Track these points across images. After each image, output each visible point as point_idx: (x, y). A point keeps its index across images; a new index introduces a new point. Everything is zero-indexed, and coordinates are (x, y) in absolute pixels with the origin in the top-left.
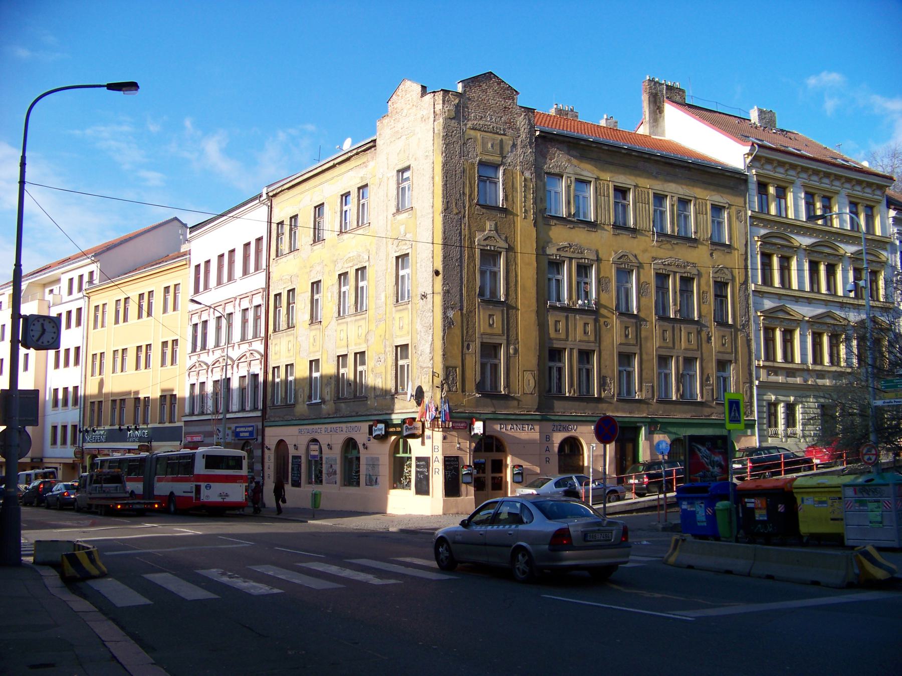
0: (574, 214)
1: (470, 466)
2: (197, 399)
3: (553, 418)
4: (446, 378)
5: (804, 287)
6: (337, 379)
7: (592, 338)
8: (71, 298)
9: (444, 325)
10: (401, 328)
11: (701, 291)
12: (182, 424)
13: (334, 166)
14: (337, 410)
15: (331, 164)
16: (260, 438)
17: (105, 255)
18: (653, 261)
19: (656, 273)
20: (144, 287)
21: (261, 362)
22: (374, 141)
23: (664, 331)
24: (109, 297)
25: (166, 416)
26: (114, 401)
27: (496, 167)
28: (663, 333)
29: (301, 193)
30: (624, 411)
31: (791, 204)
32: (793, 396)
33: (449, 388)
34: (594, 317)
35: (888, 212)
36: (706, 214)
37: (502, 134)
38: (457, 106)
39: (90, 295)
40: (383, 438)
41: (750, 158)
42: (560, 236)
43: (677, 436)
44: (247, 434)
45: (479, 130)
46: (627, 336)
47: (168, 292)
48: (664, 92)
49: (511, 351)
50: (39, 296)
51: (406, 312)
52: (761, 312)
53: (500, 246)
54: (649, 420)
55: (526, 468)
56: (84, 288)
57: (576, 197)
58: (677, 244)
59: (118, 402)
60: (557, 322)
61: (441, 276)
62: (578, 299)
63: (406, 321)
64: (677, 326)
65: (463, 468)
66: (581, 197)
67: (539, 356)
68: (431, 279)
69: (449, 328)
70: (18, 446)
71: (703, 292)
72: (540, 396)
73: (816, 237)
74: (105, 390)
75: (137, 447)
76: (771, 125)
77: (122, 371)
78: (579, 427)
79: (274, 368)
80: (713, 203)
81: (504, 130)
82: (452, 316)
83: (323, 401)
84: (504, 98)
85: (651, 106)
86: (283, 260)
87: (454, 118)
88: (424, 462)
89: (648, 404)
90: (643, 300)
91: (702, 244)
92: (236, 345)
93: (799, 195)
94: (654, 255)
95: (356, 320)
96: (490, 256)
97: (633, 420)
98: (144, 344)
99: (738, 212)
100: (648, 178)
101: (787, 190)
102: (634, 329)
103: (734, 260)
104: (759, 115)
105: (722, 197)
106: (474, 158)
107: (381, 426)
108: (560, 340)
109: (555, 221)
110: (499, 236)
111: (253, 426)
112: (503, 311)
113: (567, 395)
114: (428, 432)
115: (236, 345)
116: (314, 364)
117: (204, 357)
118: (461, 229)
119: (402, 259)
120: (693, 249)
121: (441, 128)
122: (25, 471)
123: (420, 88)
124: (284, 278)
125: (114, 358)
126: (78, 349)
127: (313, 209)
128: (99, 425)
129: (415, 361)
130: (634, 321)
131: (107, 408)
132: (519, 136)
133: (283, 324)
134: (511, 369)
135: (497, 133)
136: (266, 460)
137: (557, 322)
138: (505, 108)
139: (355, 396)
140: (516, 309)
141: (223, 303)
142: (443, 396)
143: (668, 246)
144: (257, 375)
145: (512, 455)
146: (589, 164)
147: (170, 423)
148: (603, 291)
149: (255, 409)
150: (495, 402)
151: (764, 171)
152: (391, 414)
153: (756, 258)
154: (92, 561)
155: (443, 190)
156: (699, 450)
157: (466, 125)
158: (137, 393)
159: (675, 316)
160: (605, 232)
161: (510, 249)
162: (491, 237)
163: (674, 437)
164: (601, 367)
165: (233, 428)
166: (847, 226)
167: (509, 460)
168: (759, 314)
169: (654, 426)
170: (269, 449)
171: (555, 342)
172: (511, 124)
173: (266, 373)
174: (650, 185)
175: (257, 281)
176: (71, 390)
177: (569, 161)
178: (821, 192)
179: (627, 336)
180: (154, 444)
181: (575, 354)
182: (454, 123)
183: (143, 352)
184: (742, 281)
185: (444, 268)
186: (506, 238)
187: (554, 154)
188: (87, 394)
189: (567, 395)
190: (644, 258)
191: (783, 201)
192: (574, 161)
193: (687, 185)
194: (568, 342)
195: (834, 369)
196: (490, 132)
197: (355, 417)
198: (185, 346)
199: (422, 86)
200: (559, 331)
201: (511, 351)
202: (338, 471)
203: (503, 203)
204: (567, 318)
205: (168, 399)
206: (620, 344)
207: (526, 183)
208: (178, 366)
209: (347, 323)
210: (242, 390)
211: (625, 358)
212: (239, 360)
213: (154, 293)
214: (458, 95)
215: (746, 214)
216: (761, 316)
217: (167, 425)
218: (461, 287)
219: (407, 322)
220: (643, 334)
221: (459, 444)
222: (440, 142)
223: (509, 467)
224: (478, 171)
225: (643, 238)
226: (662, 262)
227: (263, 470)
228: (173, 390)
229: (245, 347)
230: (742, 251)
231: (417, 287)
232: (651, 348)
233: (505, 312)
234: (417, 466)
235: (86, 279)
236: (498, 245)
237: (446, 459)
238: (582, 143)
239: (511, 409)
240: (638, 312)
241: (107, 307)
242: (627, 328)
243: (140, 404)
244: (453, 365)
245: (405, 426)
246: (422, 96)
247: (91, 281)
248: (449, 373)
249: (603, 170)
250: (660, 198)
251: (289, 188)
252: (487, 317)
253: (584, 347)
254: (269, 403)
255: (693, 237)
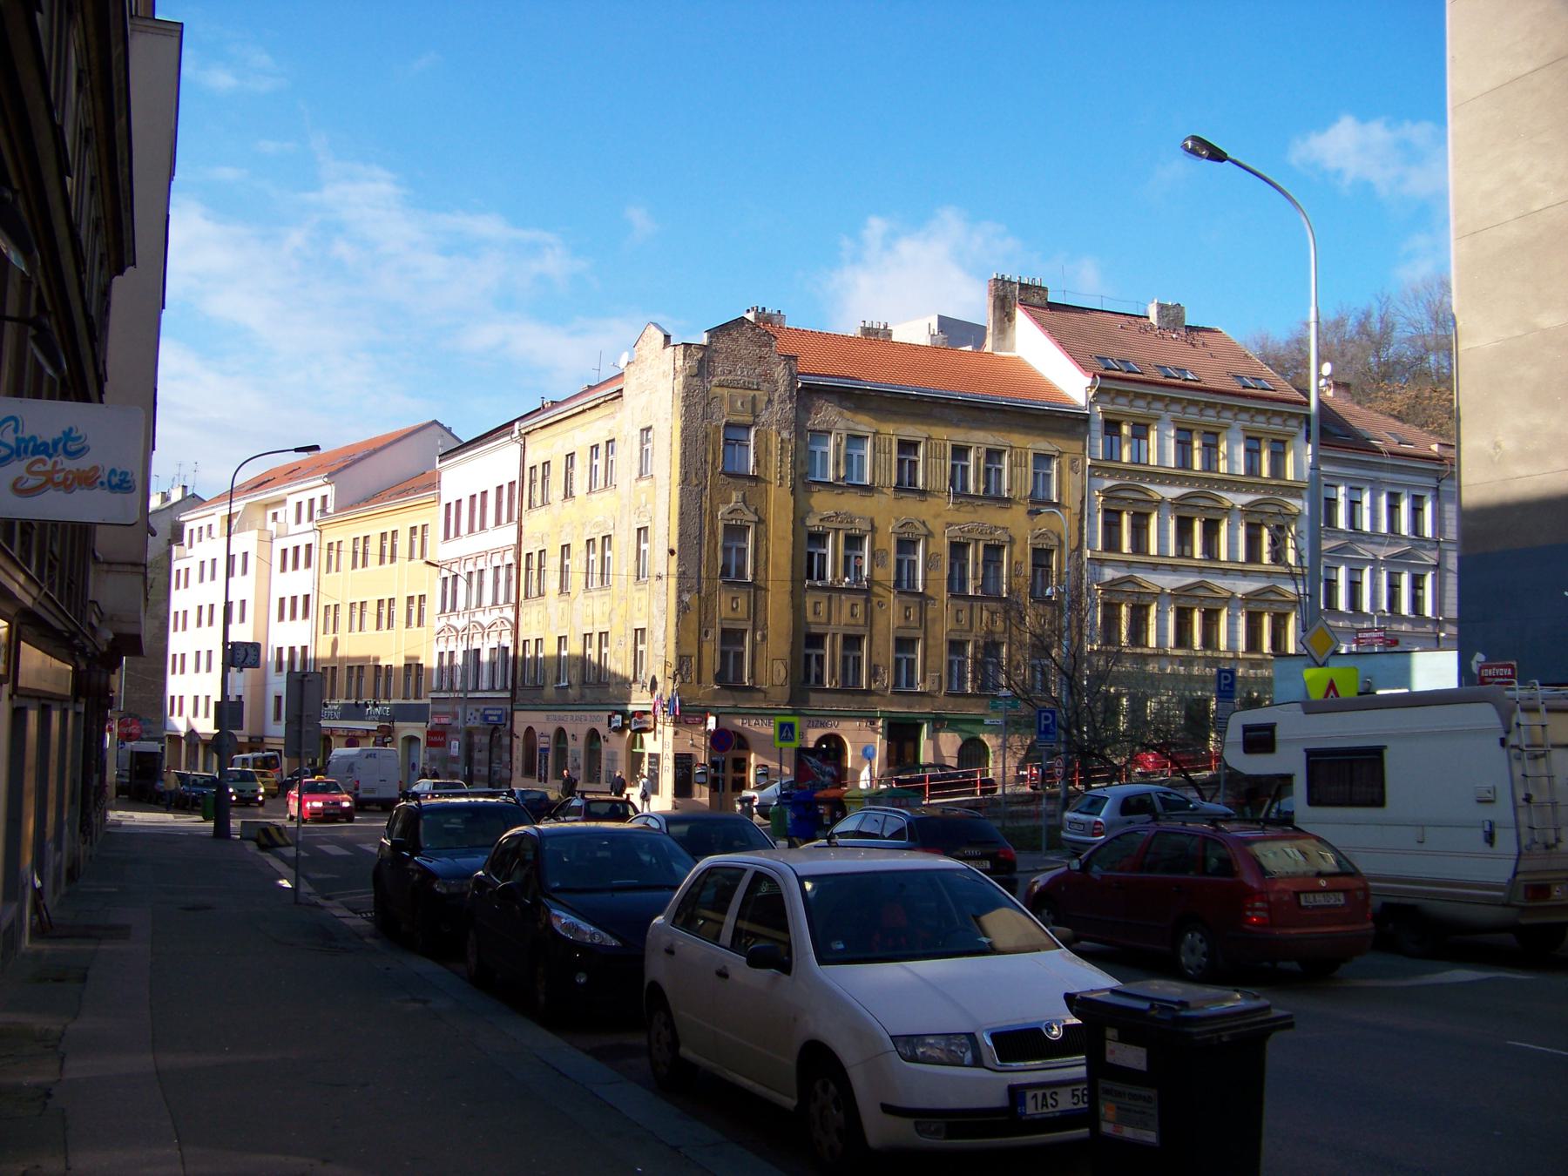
0: (844, 477)
1: (705, 765)
2: (446, 671)
3: (807, 712)
5: (1167, 551)
6: (583, 660)
7: (861, 621)
8: (300, 528)
10: (639, 610)
11: (1014, 562)
12: (429, 701)
13: (583, 411)
14: (582, 696)
15: (580, 409)
16: (509, 723)
17: (339, 475)
18: (947, 528)
19: (951, 543)
20: (387, 524)
21: (511, 633)
22: (621, 390)
23: (958, 611)
24: (345, 532)
25: (412, 692)
26: (350, 668)
27: (748, 428)
28: (957, 614)
29: (553, 436)
30: (900, 705)
31: (1153, 446)
33: (683, 679)
34: (865, 597)
36: (1026, 466)
37: (755, 390)
38: (701, 361)
39: (323, 527)
40: (620, 730)
41: (1094, 391)
42: (824, 504)
43: (972, 735)
44: (495, 718)
45: (728, 387)
46: (907, 618)
47: (415, 534)
48: (1017, 293)
49: (758, 638)
50: (259, 524)
52: (1097, 585)
53: (749, 519)
54: (931, 716)
55: (773, 769)
56: (315, 518)
57: (849, 457)
58: (982, 505)
59: (355, 669)
61: (676, 556)
62: (845, 577)
63: (644, 603)
64: (977, 605)
66: (855, 457)
67: (792, 643)
69: (684, 612)
70: (228, 745)
71: (1016, 563)
72: (792, 689)
73: (1191, 486)
74: (339, 654)
75: (376, 728)
76: (1176, 324)
77: (360, 630)
78: (840, 723)
79: (525, 641)
80: (1036, 452)
81: (758, 384)
83: (570, 685)
84: (759, 346)
85: (997, 314)
86: (536, 513)
87: (696, 375)
88: (655, 758)
89: (932, 696)
90: (932, 575)
91: (1018, 503)
92: (487, 610)
93: (1167, 433)
94: (949, 520)
95: (601, 596)
96: (735, 532)
97: (911, 715)
98: (386, 598)
99: (1073, 461)
100: (946, 426)
101: (1151, 427)
102: (918, 609)
103: (1063, 522)
104: (1158, 313)
105: (1049, 443)
106: (719, 420)
107: (618, 717)
108: (820, 624)
109: (818, 487)
110: (747, 507)
111: (501, 709)
113: (828, 686)
114: (659, 727)
115: (487, 610)
116: (561, 640)
117: (454, 621)
118: (701, 502)
119: (642, 532)
120: (1004, 510)
121: (681, 387)
122: (241, 753)
123: (662, 338)
124: (536, 535)
125: (351, 613)
126: (307, 597)
127: (564, 458)
128: (332, 697)
130: (918, 600)
131: (342, 677)
132: (777, 390)
133: (535, 592)
134: (758, 656)
135: (749, 389)
136: (515, 750)
138: (760, 357)
139: (599, 681)
140: (766, 590)
141: (474, 556)
143: (969, 508)
144: (507, 648)
145: (756, 753)
146: (867, 415)
147: (415, 699)
148: (878, 566)
149: (505, 689)
150: (736, 694)
151: (1114, 406)
152: (626, 704)
153: (1096, 517)
154: (281, 835)
155: (681, 460)
156: (809, 761)
157: (711, 382)
158: (377, 659)
159: (975, 592)
161: (761, 521)
162: (737, 510)
163: (966, 736)
164: (873, 654)
165: (482, 710)
166: (1240, 470)
167: (753, 759)
169: (939, 723)
170: (518, 737)
171: (812, 626)
172: (767, 377)
173: (516, 646)
174: (947, 435)
175: (508, 534)
176: (298, 650)
177: (841, 414)
178: (1199, 428)
179: (907, 618)
180: (397, 724)
181: (839, 639)
182: (697, 381)
183: (385, 608)
184: (1074, 545)
185: (680, 546)
186: (756, 509)
187: (822, 407)
188: (317, 657)
189: (828, 686)
190: (936, 525)
191: (1143, 442)
192: (847, 414)
193: (999, 431)
194: (831, 627)
195: (1179, 652)
196: (741, 388)
197: (596, 705)
198: (433, 605)
199: (665, 336)
201: (758, 638)
202: (582, 766)
203: (753, 470)
204: (830, 598)
205: (413, 668)
206: (898, 628)
207: (784, 445)
208: (425, 629)
209: (593, 598)
210: (492, 664)
211: (904, 644)
212: (490, 628)
213: (399, 532)
214: (702, 347)
215: (1084, 462)
216: (1098, 589)
217: (412, 701)
218: (700, 567)
220: (930, 615)
221: (692, 740)
222: (679, 403)
224: (724, 434)
225: (936, 500)
226: (960, 529)
227: (511, 761)
228: (418, 658)
229: (496, 613)
230: (1077, 508)
231: (654, 566)
233: (752, 594)
234: (650, 763)
235: (318, 505)
236: (745, 518)
238: (857, 392)
239: (758, 703)
240: (924, 590)
241: (343, 545)
242: (907, 608)
243: (382, 673)
244: (687, 654)
246: (664, 348)
247: (323, 510)
249: (883, 420)
250: (960, 452)
251: (541, 428)
252: (730, 601)
253: (851, 631)
254: (519, 682)
255: (1006, 496)
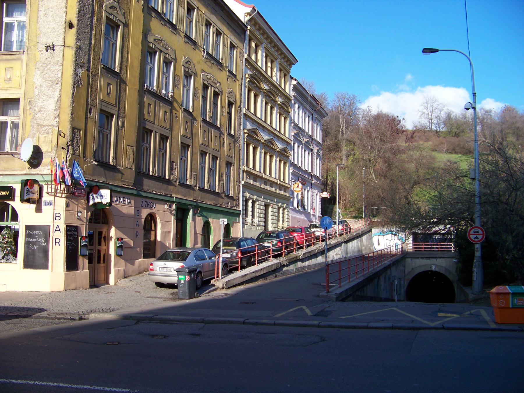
1: (86, 237)
4: (72, 140)
9: (74, 82)
32: (256, 196)
33: (74, 151)
35: (291, 81)
49: (120, 124)
51: (18, 63)
54: (195, 204)
60: (149, 105)
65: (81, 239)
68: (63, 30)
82: (81, 74)
97: (184, 202)
112: (117, 82)
114: (46, 198)
129: (29, 118)
137: (149, 105)
142: (68, 159)
160: (180, 37)
161: (126, 25)
167: (113, 232)
168: (246, 131)
185: (79, 21)
194: (154, 126)
200: (150, 114)
201: (120, 124)
211: (185, 147)
219: (18, 73)
223: (113, 240)
232: (197, 143)
237: (68, 228)
245: (26, 188)
248: (75, 135)
252: (106, 85)
